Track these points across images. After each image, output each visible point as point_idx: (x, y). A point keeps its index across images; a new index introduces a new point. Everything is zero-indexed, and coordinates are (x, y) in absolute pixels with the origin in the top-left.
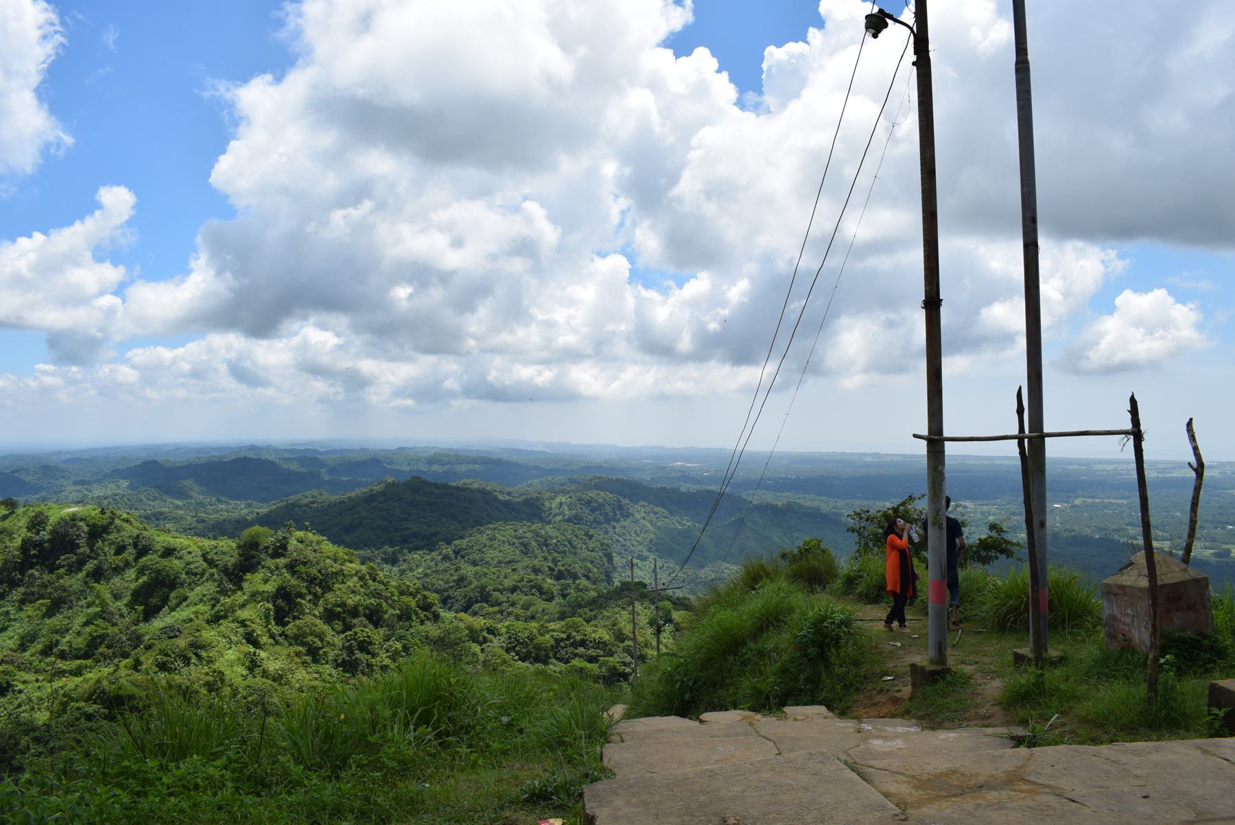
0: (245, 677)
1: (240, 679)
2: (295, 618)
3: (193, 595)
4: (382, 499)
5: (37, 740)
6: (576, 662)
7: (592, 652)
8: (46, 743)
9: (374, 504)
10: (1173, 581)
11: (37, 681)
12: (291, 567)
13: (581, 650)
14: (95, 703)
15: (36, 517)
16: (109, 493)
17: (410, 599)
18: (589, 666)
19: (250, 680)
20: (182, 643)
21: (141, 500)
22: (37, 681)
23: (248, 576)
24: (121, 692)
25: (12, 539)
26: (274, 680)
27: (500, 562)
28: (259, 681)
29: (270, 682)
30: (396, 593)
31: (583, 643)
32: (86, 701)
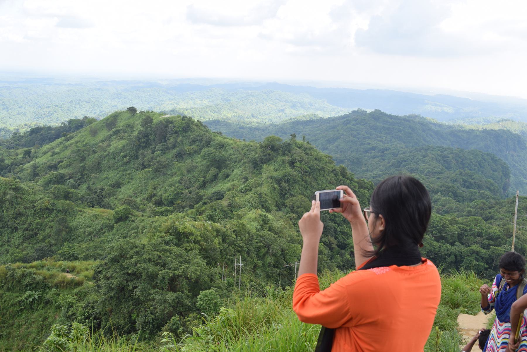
0: (258, 230)
1: (255, 231)
2: (292, 195)
3: (190, 316)
4: (353, 123)
5: (137, 253)
6: (474, 247)
7: (486, 242)
8: (142, 256)
9: (349, 126)
10: (326, 116)
11: (143, 216)
12: (292, 164)
13: (479, 239)
14: (170, 235)
15: (146, 119)
16: (189, 107)
17: (366, 191)
18: (484, 251)
19: (262, 233)
20: (224, 203)
21: (207, 112)
22: (143, 216)
23: (265, 166)
24: (185, 230)
25: (132, 131)
26: (276, 233)
27: (429, 172)
28: (265, 233)
29: (273, 234)
30: (357, 187)
31: (480, 235)
32: (166, 233)
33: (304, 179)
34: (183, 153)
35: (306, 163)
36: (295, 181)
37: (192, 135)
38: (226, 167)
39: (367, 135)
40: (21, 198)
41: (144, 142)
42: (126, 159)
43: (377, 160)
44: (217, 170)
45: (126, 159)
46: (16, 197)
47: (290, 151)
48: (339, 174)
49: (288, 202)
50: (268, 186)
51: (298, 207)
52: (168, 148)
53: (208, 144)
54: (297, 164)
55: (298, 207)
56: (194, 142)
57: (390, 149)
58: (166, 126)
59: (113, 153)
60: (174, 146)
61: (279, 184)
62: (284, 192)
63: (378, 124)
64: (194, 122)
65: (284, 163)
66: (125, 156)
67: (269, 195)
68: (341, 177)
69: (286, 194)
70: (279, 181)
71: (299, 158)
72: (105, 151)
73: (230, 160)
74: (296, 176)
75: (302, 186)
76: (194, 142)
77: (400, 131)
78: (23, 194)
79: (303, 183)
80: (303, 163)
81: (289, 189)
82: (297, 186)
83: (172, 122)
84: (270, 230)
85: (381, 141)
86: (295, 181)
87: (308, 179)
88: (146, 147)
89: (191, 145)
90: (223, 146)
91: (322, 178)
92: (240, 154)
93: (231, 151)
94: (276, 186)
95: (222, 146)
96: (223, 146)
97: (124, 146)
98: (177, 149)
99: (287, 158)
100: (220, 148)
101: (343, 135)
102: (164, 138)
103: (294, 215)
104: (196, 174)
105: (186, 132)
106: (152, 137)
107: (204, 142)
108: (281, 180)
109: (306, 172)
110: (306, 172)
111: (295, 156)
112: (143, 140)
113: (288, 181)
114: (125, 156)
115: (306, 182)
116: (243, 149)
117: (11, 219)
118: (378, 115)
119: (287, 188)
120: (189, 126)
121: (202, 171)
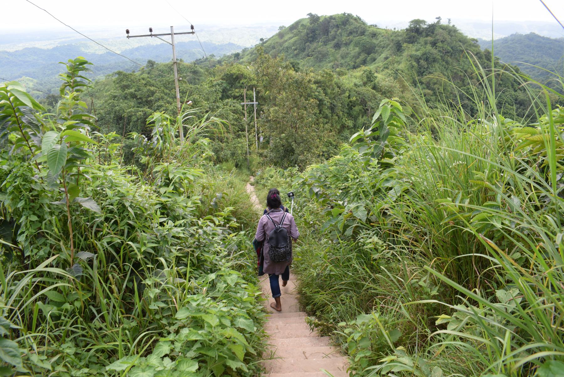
2: (430, 73)
12: (434, 44)
33: (446, 59)
34: (340, 43)
35: (449, 44)
36: (435, 60)
37: (349, 28)
38: (375, 53)
39: (521, 52)
40: (198, 79)
41: (312, 37)
42: (296, 52)
43: (528, 70)
44: (366, 55)
45: (296, 52)
46: (195, 79)
47: (433, 33)
48: (484, 57)
49: (425, 79)
50: (406, 64)
51: (435, 84)
52: (329, 40)
53: (363, 33)
54: (439, 44)
55: (435, 84)
56: (351, 33)
57: (540, 62)
58: (329, 22)
59: (287, 48)
60: (334, 38)
61: (418, 62)
62: (422, 70)
63: (532, 43)
64: (353, 16)
65: (426, 43)
66: (296, 50)
67: (406, 71)
68: (485, 61)
69: (424, 72)
70: (418, 60)
71: (441, 38)
72: (281, 46)
73: (379, 47)
74: (436, 54)
75: (443, 65)
76: (351, 33)
77: (550, 49)
78: (200, 76)
79: (444, 63)
80: (445, 43)
81: (428, 67)
82: (437, 65)
83: (334, 19)
84: (374, 88)
85: (533, 57)
86: (435, 60)
87: (449, 59)
88: (313, 41)
89: (348, 36)
90: (375, 35)
91: (465, 60)
92: (389, 40)
93: (381, 39)
94: (415, 64)
95: (374, 35)
96: (375, 35)
97: (296, 41)
98: (336, 40)
99: (429, 38)
100: (372, 37)
101: (501, 51)
102: (326, 31)
103: (429, 91)
104: (348, 59)
105: (345, 26)
106: (317, 32)
107: (359, 33)
108: (420, 58)
109: (448, 52)
110: (448, 52)
111: (438, 37)
112: (311, 35)
113: (427, 59)
114: (296, 50)
115: (447, 62)
116: (391, 36)
117: (298, 120)
118: (532, 37)
119: (426, 66)
120: (348, 20)
121: (354, 57)
